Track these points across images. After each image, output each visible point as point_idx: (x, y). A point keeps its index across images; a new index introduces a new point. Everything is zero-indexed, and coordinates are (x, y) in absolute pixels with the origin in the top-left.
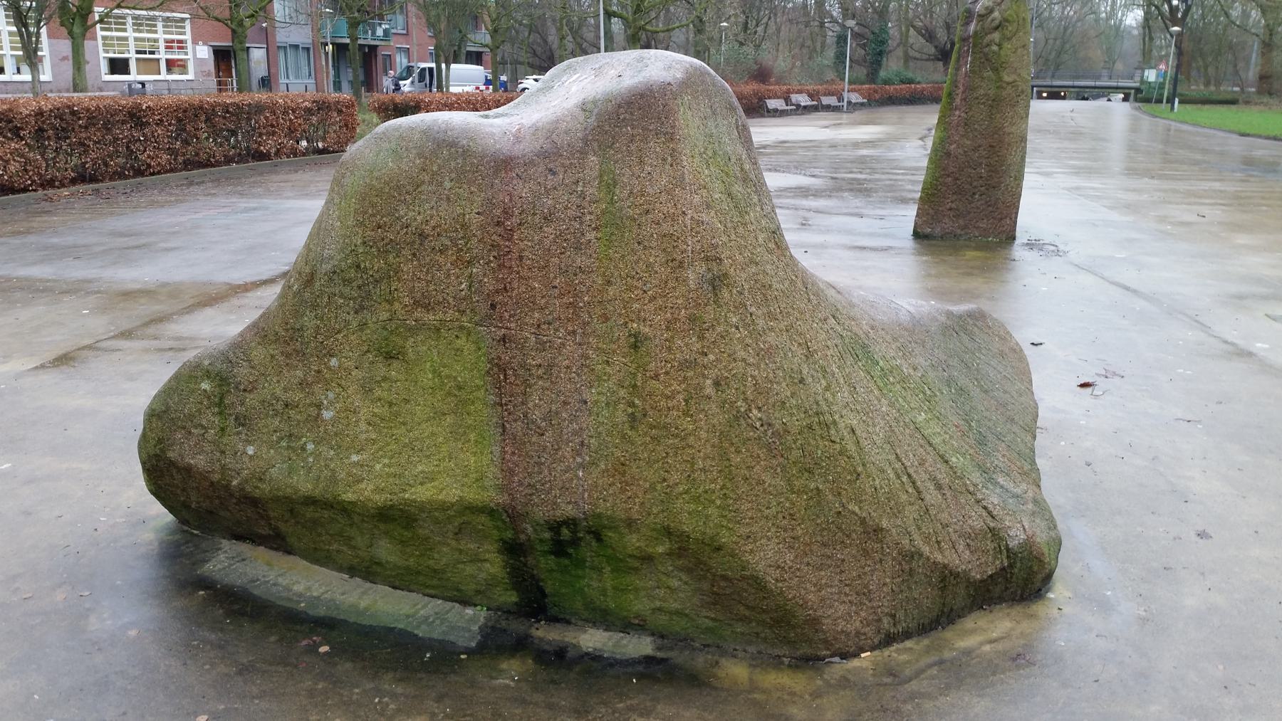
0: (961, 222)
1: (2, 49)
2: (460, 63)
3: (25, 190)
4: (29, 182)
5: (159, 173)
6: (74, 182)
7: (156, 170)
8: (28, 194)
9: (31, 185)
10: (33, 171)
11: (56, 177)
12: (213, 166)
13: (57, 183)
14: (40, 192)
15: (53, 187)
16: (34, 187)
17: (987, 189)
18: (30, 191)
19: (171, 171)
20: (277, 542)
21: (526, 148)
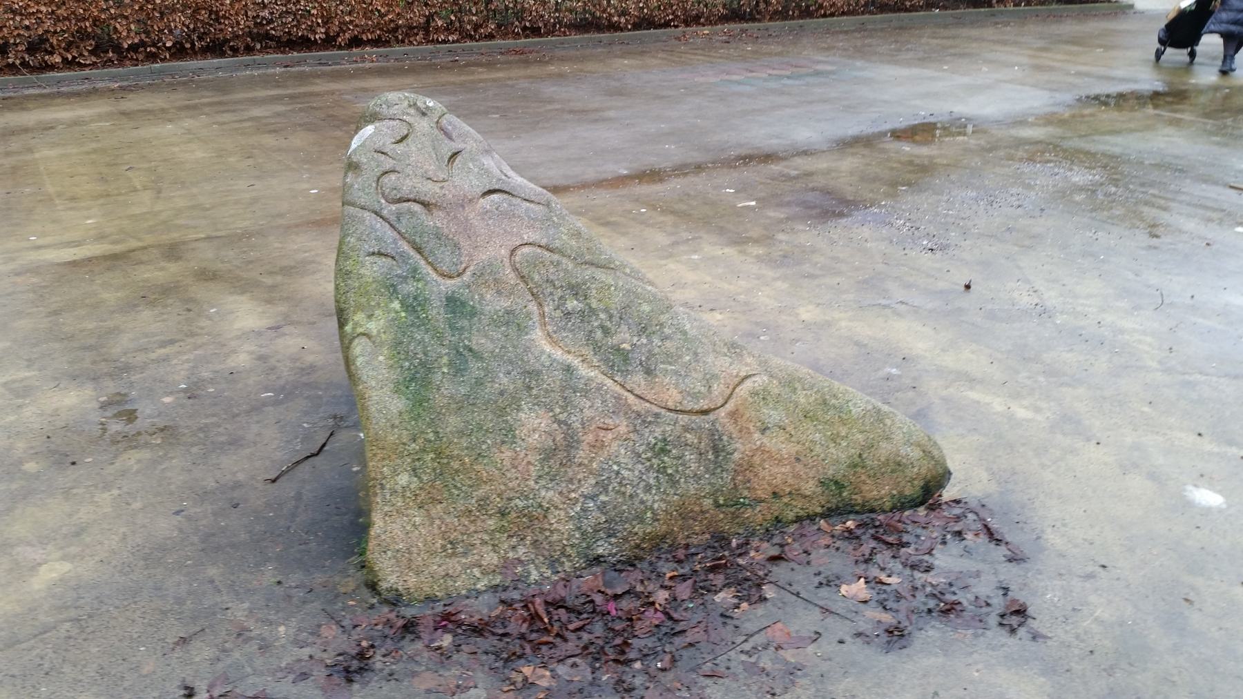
0: (159, 498)
1: (480, 697)
2: (1076, 3)
3: (667, 25)
4: (671, 17)
5: (832, 15)
6: (724, 19)
7: (828, 12)
8: (668, 30)
9: (672, 20)
10: (678, 4)
11: (703, 13)
12: (907, 10)
13: (702, 20)
14: (680, 28)
15: (698, 24)
16: (676, 23)
17: (390, 456)
18: (671, 26)
19: (843, 13)
20: (74, 264)
21: (1146, 94)
